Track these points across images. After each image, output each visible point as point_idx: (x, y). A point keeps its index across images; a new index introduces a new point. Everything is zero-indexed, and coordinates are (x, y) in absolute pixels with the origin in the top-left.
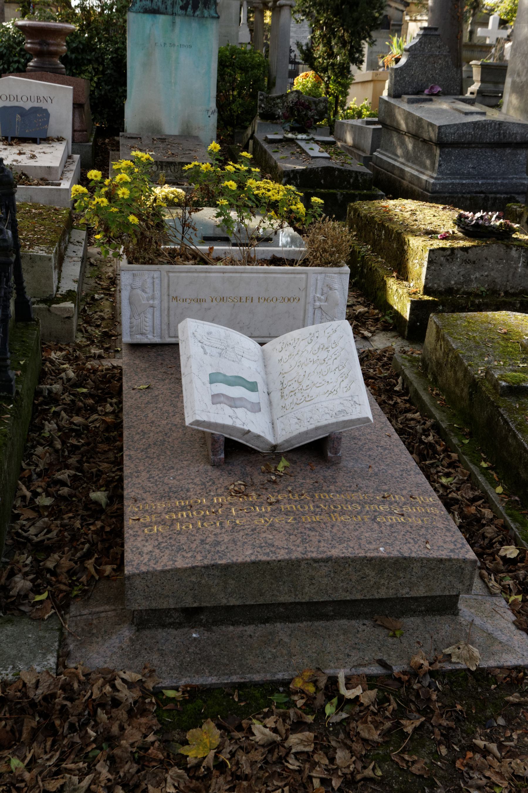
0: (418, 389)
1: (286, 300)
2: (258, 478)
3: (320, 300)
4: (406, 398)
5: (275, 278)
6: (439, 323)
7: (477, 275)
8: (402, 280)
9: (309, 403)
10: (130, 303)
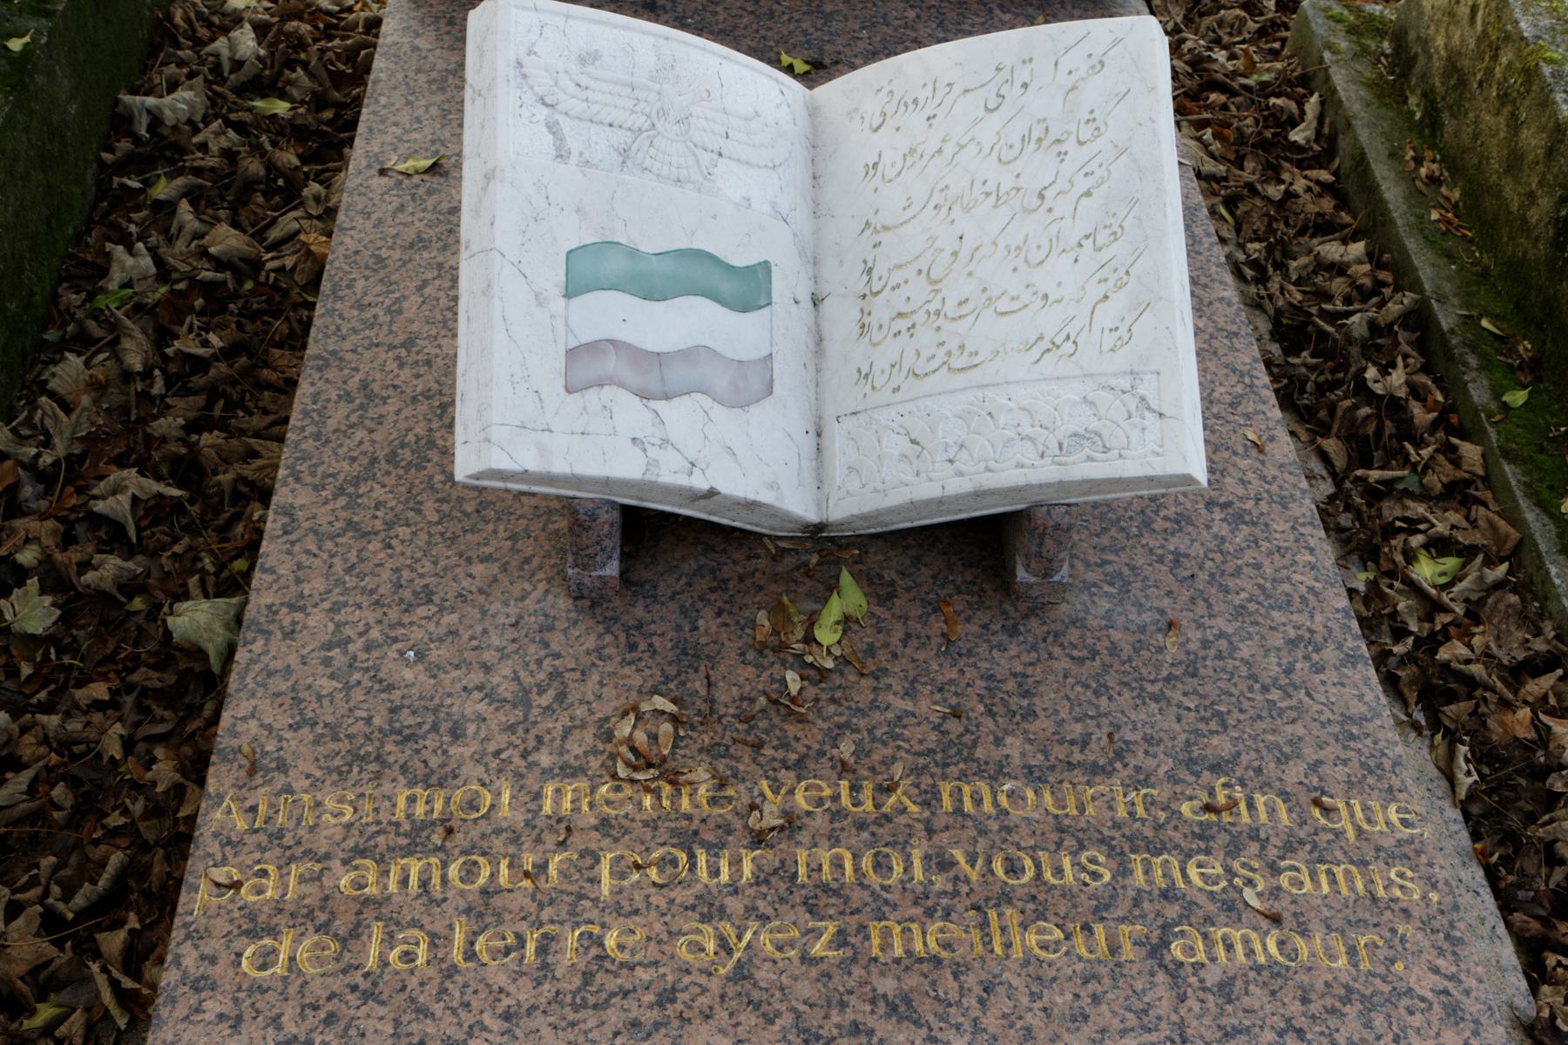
0: (1371, 156)
2: (737, 679)
4: (1325, 176)
9: (960, 380)
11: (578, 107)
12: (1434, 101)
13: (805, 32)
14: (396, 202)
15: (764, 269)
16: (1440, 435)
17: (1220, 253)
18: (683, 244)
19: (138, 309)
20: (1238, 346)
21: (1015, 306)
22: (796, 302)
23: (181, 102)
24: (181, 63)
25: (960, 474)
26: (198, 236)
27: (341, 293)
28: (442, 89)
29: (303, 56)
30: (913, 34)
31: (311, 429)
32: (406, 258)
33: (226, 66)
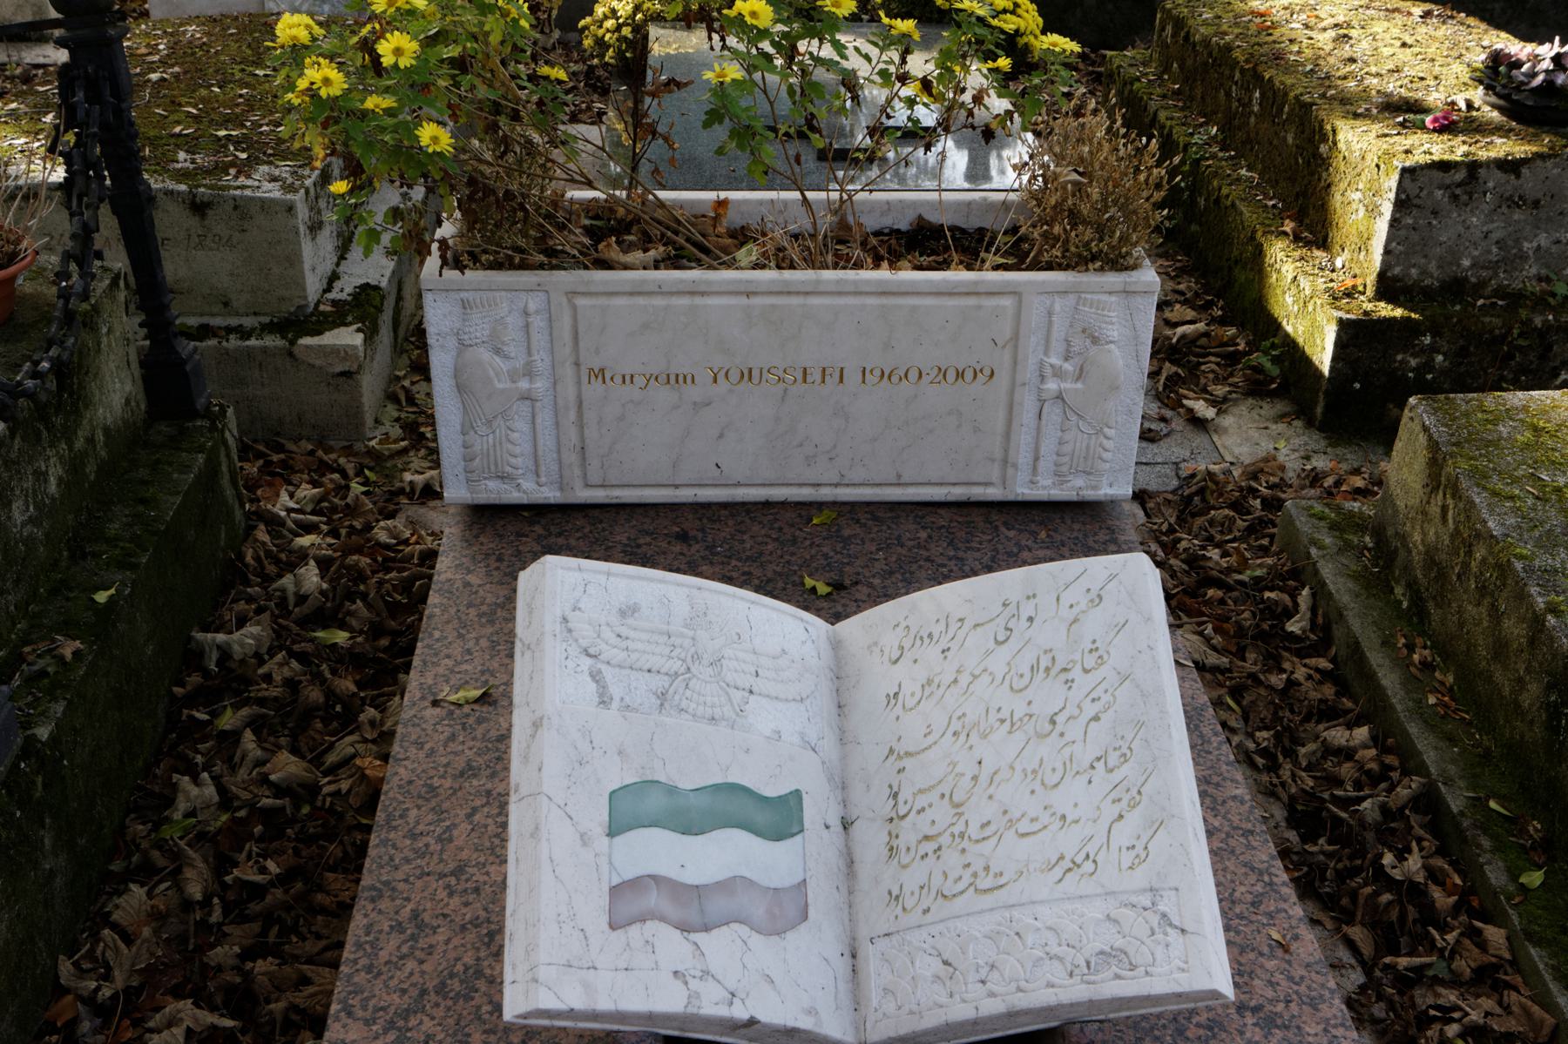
0: (1365, 644)
1: (951, 375)
3: (1058, 373)
4: (1323, 663)
5: (914, 308)
6: (1440, 432)
7: (1543, 239)
8: (1309, 244)
9: (988, 901)
10: (460, 388)
11: (619, 656)
12: (1418, 591)
13: (826, 556)
14: (448, 731)
15: (795, 799)
16: (1463, 918)
17: (1228, 753)
18: (718, 779)
19: (202, 836)
20: (1255, 844)
21: (1036, 826)
22: (827, 827)
23: (248, 637)
24: (250, 600)
25: (992, 995)
26: (260, 763)
27: (394, 823)
28: (492, 622)
29: (362, 587)
30: (925, 554)
31: (364, 962)
32: (457, 786)
33: (291, 600)
